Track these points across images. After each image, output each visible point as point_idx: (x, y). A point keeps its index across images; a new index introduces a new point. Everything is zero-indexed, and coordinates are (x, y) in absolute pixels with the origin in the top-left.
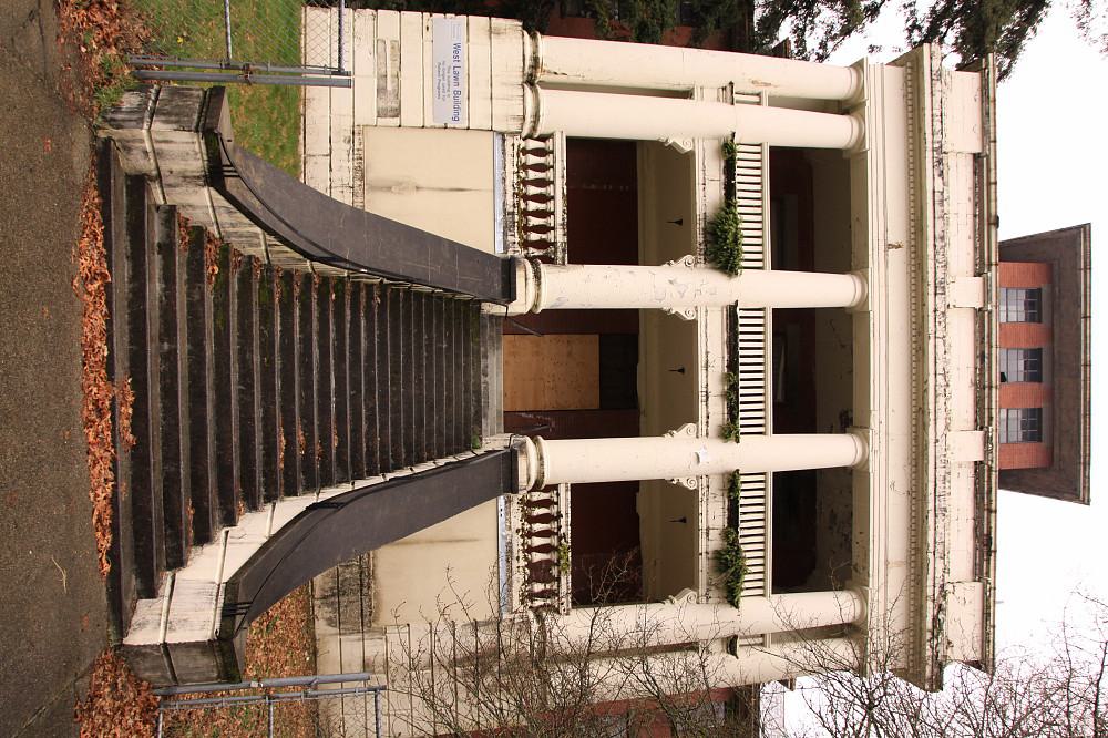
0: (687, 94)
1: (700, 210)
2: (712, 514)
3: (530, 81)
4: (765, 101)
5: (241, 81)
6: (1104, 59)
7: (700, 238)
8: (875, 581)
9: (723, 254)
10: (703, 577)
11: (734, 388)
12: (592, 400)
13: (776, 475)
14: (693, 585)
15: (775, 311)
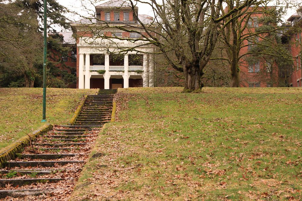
0: (84, 76)
1: (98, 75)
2: (133, 74)
4: (85, 66)
7: (101, 75)
9: (103, 72)
10: (140, 75)
11: (118, 71)
12: (121, 85)
13: (90, 65)
15: (90, 65)
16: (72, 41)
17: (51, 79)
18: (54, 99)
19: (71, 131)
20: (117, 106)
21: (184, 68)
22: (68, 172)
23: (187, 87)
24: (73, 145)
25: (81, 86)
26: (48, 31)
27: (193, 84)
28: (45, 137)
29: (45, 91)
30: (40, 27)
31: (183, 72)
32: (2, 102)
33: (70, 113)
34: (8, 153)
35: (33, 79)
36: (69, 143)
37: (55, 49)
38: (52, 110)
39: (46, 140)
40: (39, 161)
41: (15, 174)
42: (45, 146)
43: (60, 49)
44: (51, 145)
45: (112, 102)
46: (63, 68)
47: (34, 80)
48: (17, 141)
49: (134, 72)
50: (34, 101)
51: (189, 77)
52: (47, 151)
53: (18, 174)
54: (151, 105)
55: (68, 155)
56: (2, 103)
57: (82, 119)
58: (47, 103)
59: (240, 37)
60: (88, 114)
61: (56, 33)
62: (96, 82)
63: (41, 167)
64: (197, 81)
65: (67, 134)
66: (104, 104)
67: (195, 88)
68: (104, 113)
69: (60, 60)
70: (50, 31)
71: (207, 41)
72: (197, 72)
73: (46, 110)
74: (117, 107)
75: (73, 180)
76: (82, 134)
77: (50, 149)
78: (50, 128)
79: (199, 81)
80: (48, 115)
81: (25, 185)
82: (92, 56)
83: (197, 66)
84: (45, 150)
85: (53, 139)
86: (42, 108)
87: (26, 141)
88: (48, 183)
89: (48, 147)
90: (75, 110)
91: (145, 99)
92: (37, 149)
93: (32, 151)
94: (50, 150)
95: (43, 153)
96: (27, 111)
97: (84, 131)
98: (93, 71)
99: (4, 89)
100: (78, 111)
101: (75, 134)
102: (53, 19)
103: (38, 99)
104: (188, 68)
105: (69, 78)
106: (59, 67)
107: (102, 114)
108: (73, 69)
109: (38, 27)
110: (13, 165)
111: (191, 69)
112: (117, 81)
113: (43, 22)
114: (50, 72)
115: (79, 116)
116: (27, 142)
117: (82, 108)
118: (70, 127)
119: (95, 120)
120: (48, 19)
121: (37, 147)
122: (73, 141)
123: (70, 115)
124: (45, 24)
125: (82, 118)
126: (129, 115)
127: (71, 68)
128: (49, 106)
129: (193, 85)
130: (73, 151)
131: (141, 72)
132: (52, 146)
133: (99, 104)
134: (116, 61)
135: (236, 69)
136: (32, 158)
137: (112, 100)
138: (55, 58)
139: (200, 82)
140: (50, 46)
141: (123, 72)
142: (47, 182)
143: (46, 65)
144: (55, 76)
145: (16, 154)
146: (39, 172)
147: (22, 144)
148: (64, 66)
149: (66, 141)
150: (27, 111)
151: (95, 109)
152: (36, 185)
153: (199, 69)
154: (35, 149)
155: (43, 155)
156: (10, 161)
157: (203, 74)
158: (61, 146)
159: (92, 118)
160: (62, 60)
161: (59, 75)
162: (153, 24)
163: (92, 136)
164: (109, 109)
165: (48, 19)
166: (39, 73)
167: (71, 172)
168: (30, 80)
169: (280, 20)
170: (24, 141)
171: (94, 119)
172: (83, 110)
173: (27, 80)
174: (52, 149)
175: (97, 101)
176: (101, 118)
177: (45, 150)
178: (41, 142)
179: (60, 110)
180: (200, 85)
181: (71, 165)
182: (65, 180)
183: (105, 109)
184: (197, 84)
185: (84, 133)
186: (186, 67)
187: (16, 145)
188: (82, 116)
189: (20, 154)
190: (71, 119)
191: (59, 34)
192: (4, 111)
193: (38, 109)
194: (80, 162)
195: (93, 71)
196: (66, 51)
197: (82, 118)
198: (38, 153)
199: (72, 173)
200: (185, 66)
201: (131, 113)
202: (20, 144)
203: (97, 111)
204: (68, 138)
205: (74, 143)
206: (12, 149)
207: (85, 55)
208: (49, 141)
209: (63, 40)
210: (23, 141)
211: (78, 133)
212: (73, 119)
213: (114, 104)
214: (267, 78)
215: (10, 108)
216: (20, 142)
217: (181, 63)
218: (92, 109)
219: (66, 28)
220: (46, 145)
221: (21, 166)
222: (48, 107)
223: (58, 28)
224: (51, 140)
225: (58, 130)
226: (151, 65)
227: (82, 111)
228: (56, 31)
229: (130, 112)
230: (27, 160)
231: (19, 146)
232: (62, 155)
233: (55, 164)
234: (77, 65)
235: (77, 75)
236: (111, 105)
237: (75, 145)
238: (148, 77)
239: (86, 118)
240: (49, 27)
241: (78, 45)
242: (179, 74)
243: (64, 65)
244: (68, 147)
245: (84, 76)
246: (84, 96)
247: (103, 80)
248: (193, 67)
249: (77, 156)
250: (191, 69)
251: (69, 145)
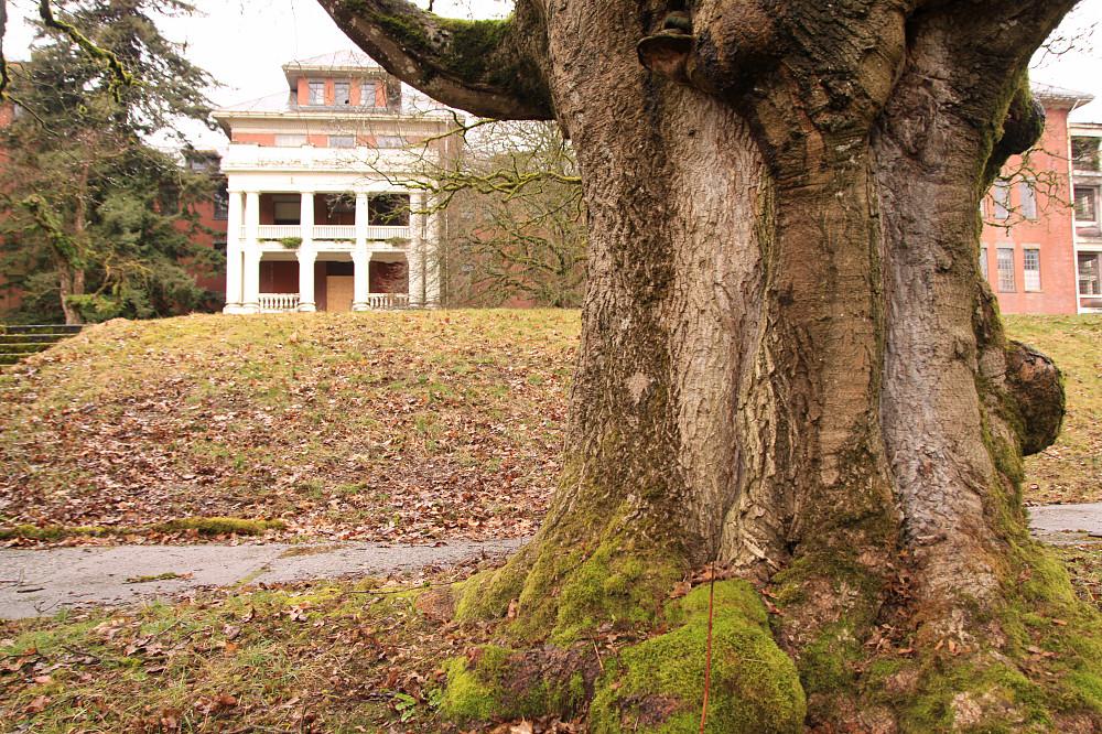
0: (243, 253)
2: (381, 247)
3: (242, 305)
5: (832, 258)
6: (27, 20)
7: (290, 250)
23: (665, 497)
27: (844, 395)
98: (268, 240)
129: (833, 437)
195: (268, 240)
207: (244, 195)
245: (243, 253)
247: (295, 265)
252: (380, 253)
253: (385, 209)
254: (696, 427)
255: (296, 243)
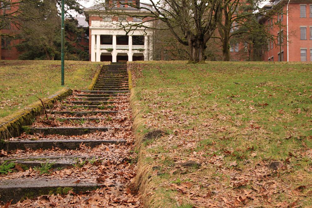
0: (96, 53)
2: (136, 52)
7: (110, 52)
8: (111, 34)
9: (111, 50)
14: (143, 53)
16: (86, 25)
17: (68, 55)
18: (72, 68)
19: (93, 96)
20: (132, 75)
21: (189, 42)
22: (106, 165)
23: (192, 59)
24: (100, 114)
25: (93, 59)
26: (65, 15)
28: (63, 103)
29: (63, 63)
30: (59, 12)
31: (188, 45)
32: (23, 70)
33: (88, 81)
34: (6, 127)
35: (53, 55)
36: (94, 110)
37: (71, 31)
38: (70, 77)
39: (66, 107)
40: (55, 139)
41: (13, 168)
42: (64, 114)
43: (75, 31)
44: (71, 114)
45: (126, 71)
46: (78, 46)
47: (54, 56)
48: (25, 108)
49: (137, 51)
50: (52, 69)
51: (194, 50)
52: (67, 121)
53: (17, 167)
54: (165, 73)
55: (97, 129)
56: (23, 71)
57: (100, 86)
58: (65, 71)
59: (231, 18)
60: (105, 81)
61: (72, 17)
62: (106, 57)
63: (58, 150)
64: (201, 54)
65: (89, 100)
66: (119, 73)
67: (199, 60)
68: (120, 81)
69: (75, 40)
70: (67, 16)
71: (218, 15)
72: (201, 45)
73: (65, 77)
74: (132, 76)
75: (121, 189)
76: (107, 99)
77: (71, 119)
78: (70, 93)
79: (203, 54)
80: (67, 83)
81: (26, 199)
82: (102, 37)
83: (202, 40)
84: (64, 121)
85: (74, 105)
86: (61, 75)
87: (38, 108)
88: (71, 194)
89: (67, 116)
90: (93, 78)
91: (157, 68)
92: (53, 119)
93: (46, 121)
94: (71, 121)
95: (62, 124)
96: (46, 78)
97: (108, 96)
99: (27, 61)
100: (96, 79)
101: (99, 99)
102: (69, 6)
103: (57, 68)
104: (193, 41)
105: (83, 55)
106: (74, 46)
107: (118, 81)
108: (86, 47)
109: (57, 12)
110: (14, 147)
111: (196, 43)
112: (122, 58)
113: (61, 8)
114: (67, 49)
115: (97, 83)
116: (40, 109)
117: (99, 76)
118: (92, 93)
119: (112, 87)
120: (65, 6)
121: (53, 115)
122: (99, 108)
123: (88, 82)
124: (63, 9)
125: (100, 85)
126: (145, 82)
127: (85, 46)
128: (67, 74)
130: (103, 122)
131: (143, 50)
132: (73, 114)
133: (114, 73)
134: (122, 40)
135: (227, 46)
136: (46, 133)
137: (126, 69)
138: (71, 38)
139: (204, 54)
140: (67, 28)
141: (128, 50)
142: (71, 192)
143: (63, 30)
144: (72, 53)
145: (23, 127)
146: (54, 162)
147: (33, 112)
148: (79, 45)
149: (90, 108)
150: (46, 78)
151: (111, 77)
152: (47, 199)
153: (203, 43)
154: (50, 119)
155: (62, 129)
156: (10, 139)
157: (206, 47)
158: (85, 114)
159: (109, 85)
160: (77, 40)
161: (75, 53)
162: (159, 4)
163: (120, 101)
164: (124, 77)
165: (65, 6)
166: (58, 50)
167: (111, 164)
168: (51, 56)
169: (258, 7)
170: (36, 108)
171: (111, 86)
172: (99, 78)
173: (48, 56)
174: (74, 119)
175: (111, 70)
176: (117, 85)
177: (64, 121)
178: (58, 109)
179: (78, 77)
180: (204, 58)
181: (106, 146)
182: (105, 188)
183: (120, 78)
184: (201, 57)
185: (109, 99)
186: (191, 41)
187: (23, 114)
188: (99, 83)
189: (28, 126)
190: (90, 86)
191: (75, 19)
192: (23, 77)
193: (57, 76)
194: (120, 142)
196: (80, 33)
197: (100, 85)
198: (55, 126)
199: (113, 166)
200: (190, 40)
201: (147, 81)
202: (29, 112)
203: (113, 79)
204: (91, 104)
205: (100, 111)
206: (14, 121)
207: (96, 36)
208: (70, 108)
209: (78, 23)
210: (35, 109)
211: (102, 99)
212: (92, 85)
213: (129, 72)
214: (246, 56)
215: (29, 75)
216: (29, 109)
217: (186, 37)
218: (108, 77)
219: (80, 13)
220: (65, 113)
221: (26, 147)
222: (66, 75)
223: (74, 13)
224: (71, 107)
225: (79, 96)
226: (151, 45)
227: (99, 79)
228: (71, 15)
229: (146, 80)
230: (38, 135)
231: (27, 116)
232: (89, 129)
233: (81, 145)
234: (90, 45)
235: (90, 52)
236: (126, 74)
237: (103, 113)
238: (148, 54)
239: (104, 85)
240: (66, 12)
241: (90, 27)
242: (185, 47)
243: (79, 44)
244: (95, 117)
245: (96, 53)
246: (99, 66)
248: (198, 41)
249: (111, 130)
250: (196, 43)
251: (96, 114)
252: (136, 53)
253: (138, 40)
254: (193, 57)
255: (111, 50)
